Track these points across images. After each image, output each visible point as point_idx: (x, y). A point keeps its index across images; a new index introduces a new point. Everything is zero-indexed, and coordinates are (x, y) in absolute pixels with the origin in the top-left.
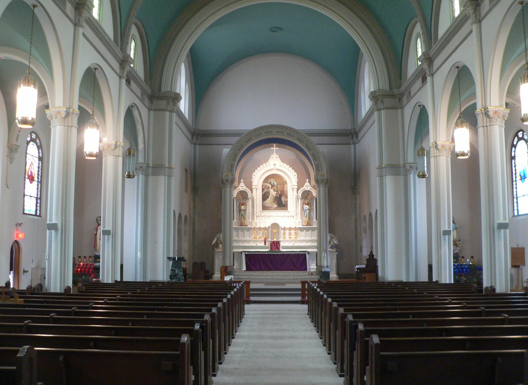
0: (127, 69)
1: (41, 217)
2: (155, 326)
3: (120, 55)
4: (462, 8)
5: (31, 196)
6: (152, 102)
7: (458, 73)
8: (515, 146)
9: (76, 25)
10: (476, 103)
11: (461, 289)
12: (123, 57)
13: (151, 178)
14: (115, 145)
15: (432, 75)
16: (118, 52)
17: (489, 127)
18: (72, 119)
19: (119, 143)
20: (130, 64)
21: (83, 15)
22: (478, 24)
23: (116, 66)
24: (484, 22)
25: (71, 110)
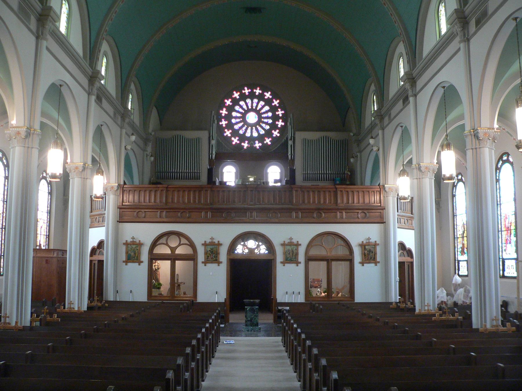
0: (97, 85)
3: (89, 71)
4: (449, 26)
7: (444, 93)
8: (500, 169)
9: (38, 37)
10: (464, 124)
11: (423, 296)
12: (92, 73)
14: (83, 167)
15: (415, 96)
16: (87, 69)
17: (478, 150)
19: (87, 165)
20: (101, 80)
21: (47, 27)
22: (467, 43)
23: (85, 82)
24: (472, 41)
25: (32, 129)
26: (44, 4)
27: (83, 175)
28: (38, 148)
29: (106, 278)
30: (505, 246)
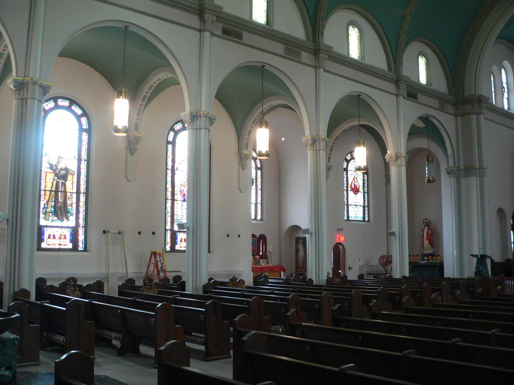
1: (370, 222)
2: (204, 300)
5: (356, 205)
6: (458, 109)
13: (463, 180)
18: (319, 145)
23: (391, 88)
26: (398, 73)
27: (397, 162)
28: (405, 165)
29: (322, 277)
30: (330, 274)
